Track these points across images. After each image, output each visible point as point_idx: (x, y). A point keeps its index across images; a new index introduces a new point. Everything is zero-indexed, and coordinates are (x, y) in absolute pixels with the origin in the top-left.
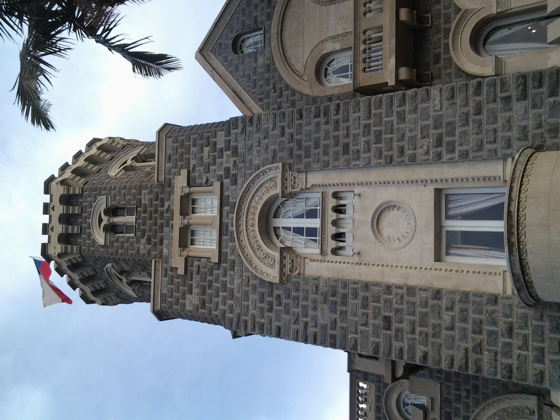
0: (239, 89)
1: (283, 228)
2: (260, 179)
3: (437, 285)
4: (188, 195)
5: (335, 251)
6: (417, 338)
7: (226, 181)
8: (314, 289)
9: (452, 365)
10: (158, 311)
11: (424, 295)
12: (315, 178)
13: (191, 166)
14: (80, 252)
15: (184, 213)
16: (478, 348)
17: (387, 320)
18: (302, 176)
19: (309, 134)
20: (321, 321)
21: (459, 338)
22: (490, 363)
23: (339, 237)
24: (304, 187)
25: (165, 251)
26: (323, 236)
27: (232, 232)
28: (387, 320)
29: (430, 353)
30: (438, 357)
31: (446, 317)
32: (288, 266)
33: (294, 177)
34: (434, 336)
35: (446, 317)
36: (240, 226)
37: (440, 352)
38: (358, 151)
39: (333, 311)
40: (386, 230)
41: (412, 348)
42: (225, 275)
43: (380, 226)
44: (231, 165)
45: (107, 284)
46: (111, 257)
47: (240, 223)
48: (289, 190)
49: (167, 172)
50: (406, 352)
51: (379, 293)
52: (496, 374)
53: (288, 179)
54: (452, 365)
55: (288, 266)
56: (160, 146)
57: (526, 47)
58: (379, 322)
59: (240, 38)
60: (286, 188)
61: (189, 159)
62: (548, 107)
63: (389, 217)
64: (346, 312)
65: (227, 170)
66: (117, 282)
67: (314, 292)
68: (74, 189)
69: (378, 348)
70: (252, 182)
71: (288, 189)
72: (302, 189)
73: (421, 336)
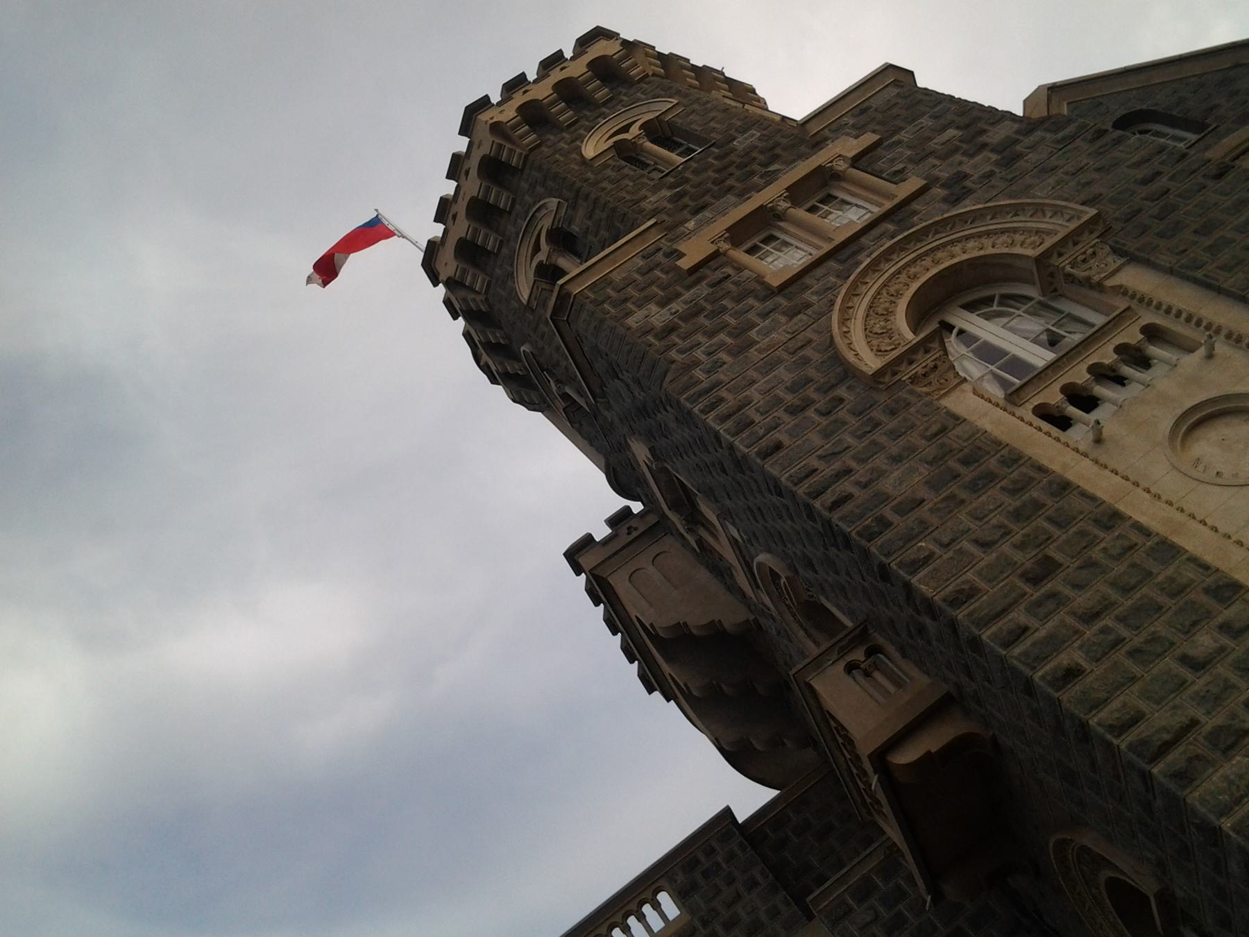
1: (961, 332)
2: (1015, 219)
4: (837, 176)
6: (1086, 636)
7: (938, 192)
8: (934, 429)
9: (1121, 728)
10: (569, 294)
11: (1189, 573)
12: (1136, 279)
13: (895, 138)
14: (531, 150)
15: (796, 193)
17: (1048, 567)
18: (1114, 262)
21: (1197, 693)
22: (1231, 783)
24: (1096, 278)
25: (691, 225)
26: (1049, 371)
27: (859, 263)
28: (1046, 569)
29: (1090, 679)
30: (1103, 695)
31: (1205, 641)
32: (917, 369)
33: (1094, 253)
34: (1134, 653)
35: (1205, 641)
36: (888, 260)
37: (1117, 688)
38: (1150, 574)
39: (934, 484)
41: (1054, 643)
42: (764, 315)
43: (1199, 433)
45: (499, 249)
46: (578, 184)
47: (894, 256)
48: (1064, 263)
49: (834, 127)
50: (1028, 642)
51: (1081, 513)
52: (1225, 811)
53: (1080, 246)
54: (1121, 728)
55: (917, 369)
56: (869, 84)
59: (1157, 122)
60: (1060, 255)
61: (754, 382)
64: (963, 501)
66: (526, 251)
67: (928, 433)
68: (635, 65)
69: (969, 597)
70: (996, 212)
71: (1062, 259)
72: (1089, 279)
73: (1102, 636)
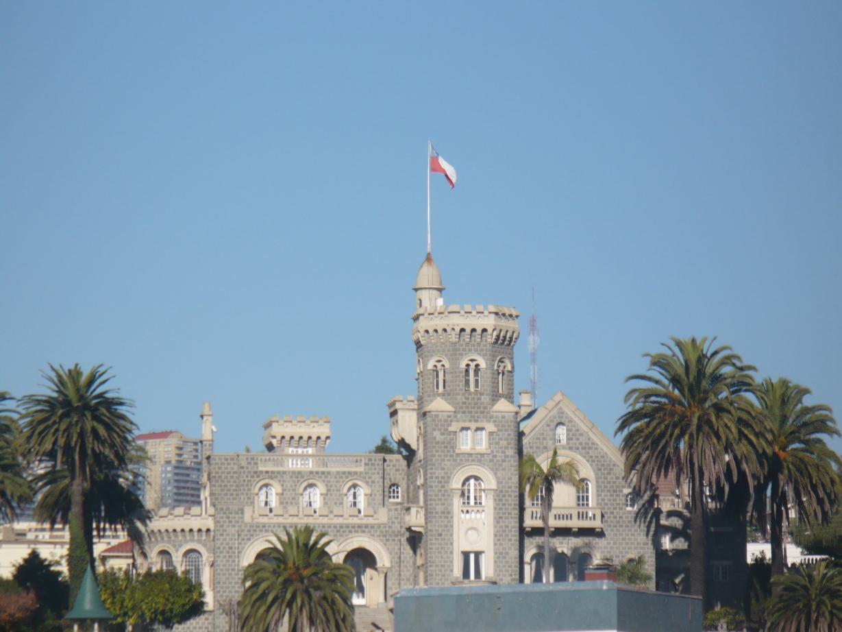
0: (537, 429)
3: (454, 553)
5: (462, 511)
16: (437, 566)
19: (507, 500)
20: (437, 507)
23: (468, 512)
28: (441, 535)
40: (470, 532)
44: (498, 458)
57: (696, 498)
58: (440, 532)
62: (100, 561)
63: (473, 531)
65: (495, 456)
